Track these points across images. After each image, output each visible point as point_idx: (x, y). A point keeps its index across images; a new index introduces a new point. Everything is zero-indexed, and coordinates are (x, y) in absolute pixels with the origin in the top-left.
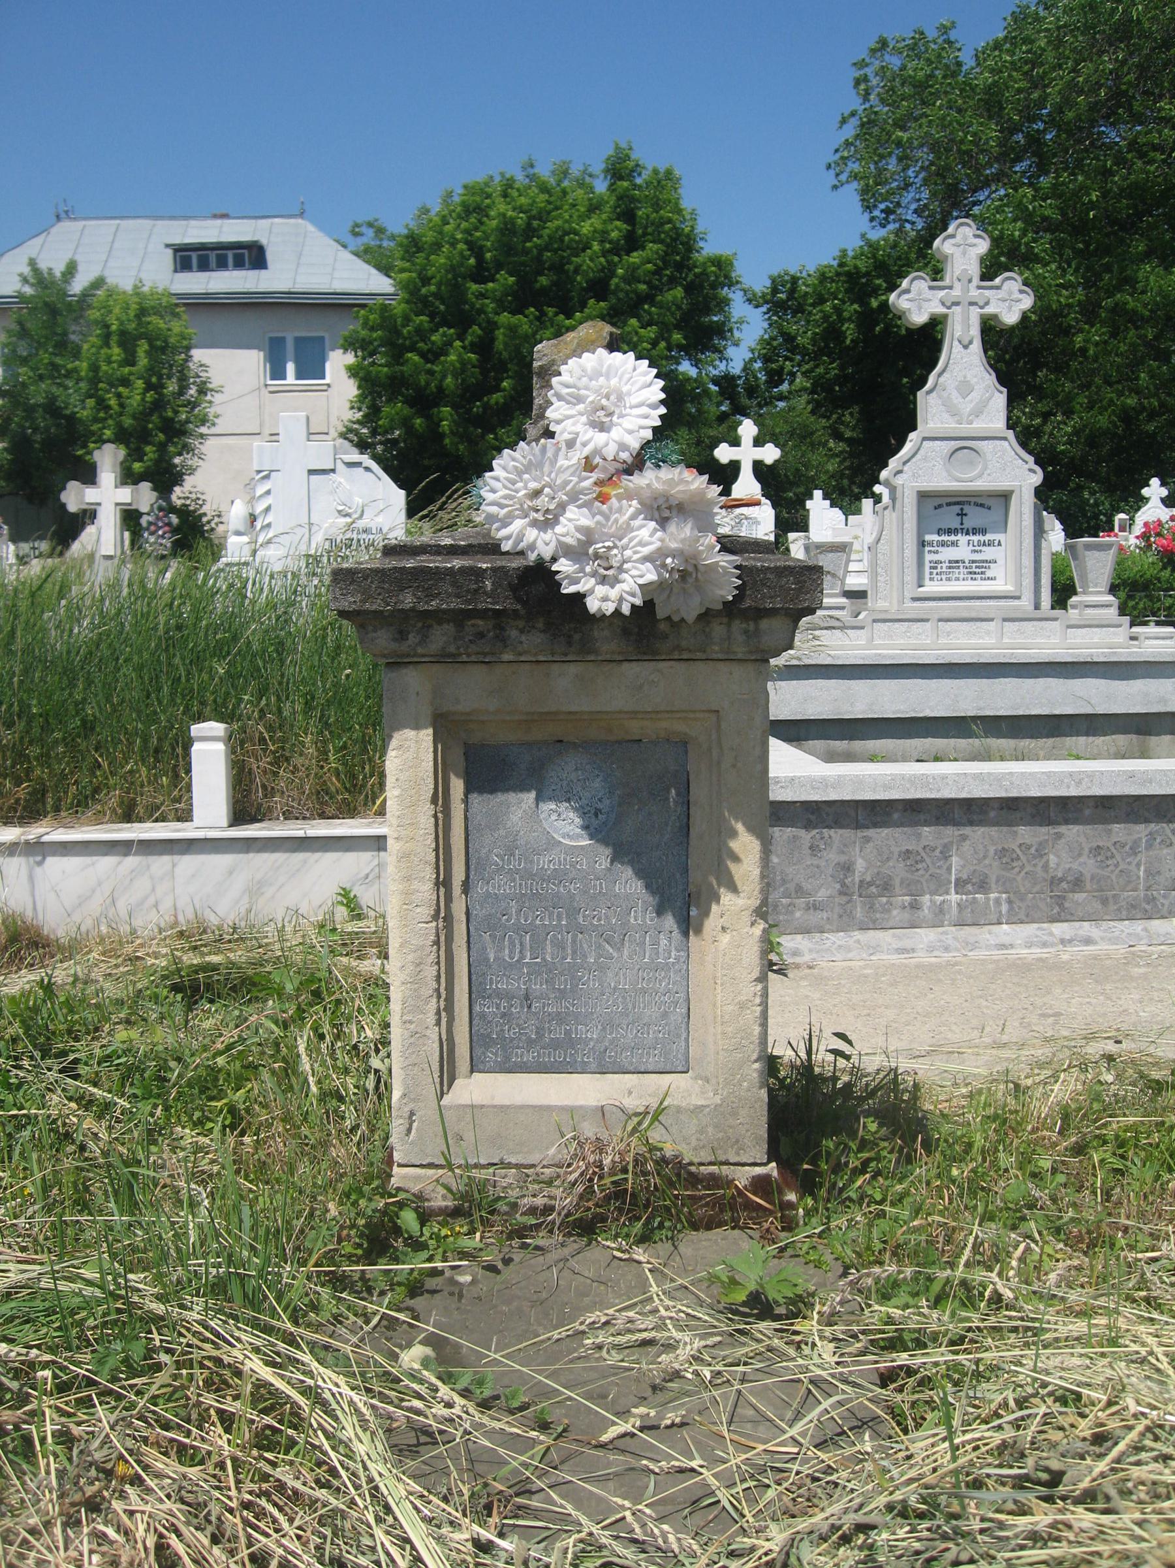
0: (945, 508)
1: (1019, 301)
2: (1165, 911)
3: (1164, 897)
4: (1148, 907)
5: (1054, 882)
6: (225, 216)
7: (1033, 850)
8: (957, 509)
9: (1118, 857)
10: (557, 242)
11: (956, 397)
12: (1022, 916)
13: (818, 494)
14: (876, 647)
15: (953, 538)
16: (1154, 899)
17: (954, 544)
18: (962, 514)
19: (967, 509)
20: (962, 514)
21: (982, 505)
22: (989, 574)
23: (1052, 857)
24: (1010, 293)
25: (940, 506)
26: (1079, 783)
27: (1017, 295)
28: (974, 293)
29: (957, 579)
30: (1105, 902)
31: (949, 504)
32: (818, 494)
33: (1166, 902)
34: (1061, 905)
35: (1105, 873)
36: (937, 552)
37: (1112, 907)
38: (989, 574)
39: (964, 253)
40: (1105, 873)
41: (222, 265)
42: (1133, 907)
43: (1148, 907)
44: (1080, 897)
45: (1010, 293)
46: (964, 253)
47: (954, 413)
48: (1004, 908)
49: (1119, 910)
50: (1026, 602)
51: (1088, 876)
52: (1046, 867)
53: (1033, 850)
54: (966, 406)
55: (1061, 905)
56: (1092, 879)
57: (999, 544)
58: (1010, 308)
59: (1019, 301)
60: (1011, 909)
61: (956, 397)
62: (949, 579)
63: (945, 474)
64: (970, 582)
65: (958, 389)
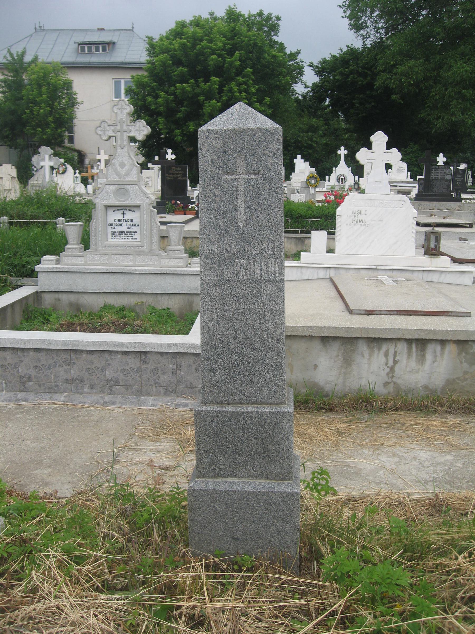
0: (117, 211)
1: (143, 130)
2: (62, 390)
3: (61, 385)
4: (55, 388)
5: (21, 377)
7: (13, 366)
8: (122, 212)
9: (44, 370)
10: (201, 53)
11: (119, 168)
12: (10, 389)
13: (299, 157)
14: (89, 265)
15: (120, 223)
16: (58, 386)
17: (121, 225)
18: (124, 214)
19: (125, 212)
20: (124, 214)
21: (131, 210)
22: (134, 237)
23: (20, 369)
24: (139, 127)
25: (115, 211)
26: (25, 343)
27: (142, 128)
28: (125, 127)
29: (122, 239)
30: (40, 386)
31: (118, 210)
32: (299, 157)
33: (62, 387)
34: (24, 386)
35: (40, 375)
36: (114, 228)
37: (42, 388)
38: (134, 237)
39: (122, 112)
40: (40, 375)
42: (50, 388)
43: (55, 388)
44: (31, 383)
45: (139, 127)
46: (122, 112)
47: (118, 174)
48: (4, 386)
49: (45, 389)
50: (145, 249)
51: (33, 377)
52: (18, 372)
53: (13, 366)
54: (123, 172)
55: (24, 386)
56: (35, 377)
57: (138, 225)
58: (140, 133)
59: (143, 130)
60: (6, 386)
61: (119, 168)
62: (119, 239)
63: (114, 199)
64: (127, 240)
65: (120, 165)
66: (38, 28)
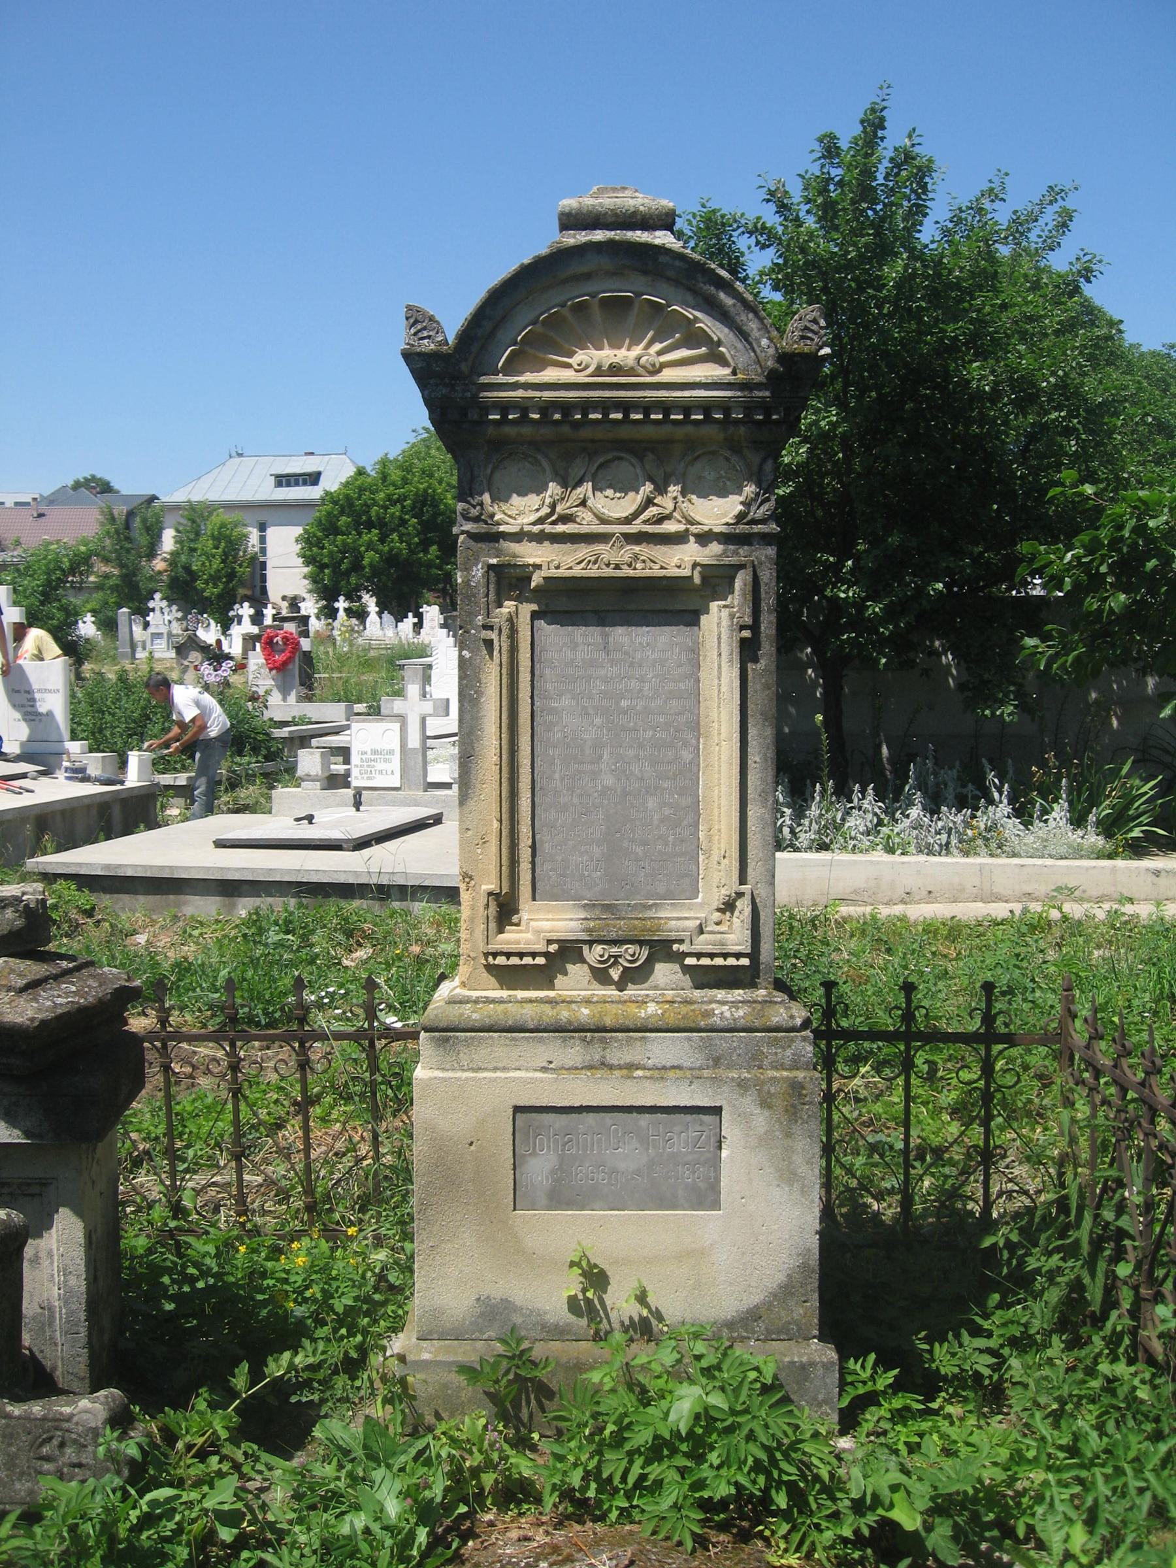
6: (312, 454)
41: (297, 484)
66: (234, 454)
